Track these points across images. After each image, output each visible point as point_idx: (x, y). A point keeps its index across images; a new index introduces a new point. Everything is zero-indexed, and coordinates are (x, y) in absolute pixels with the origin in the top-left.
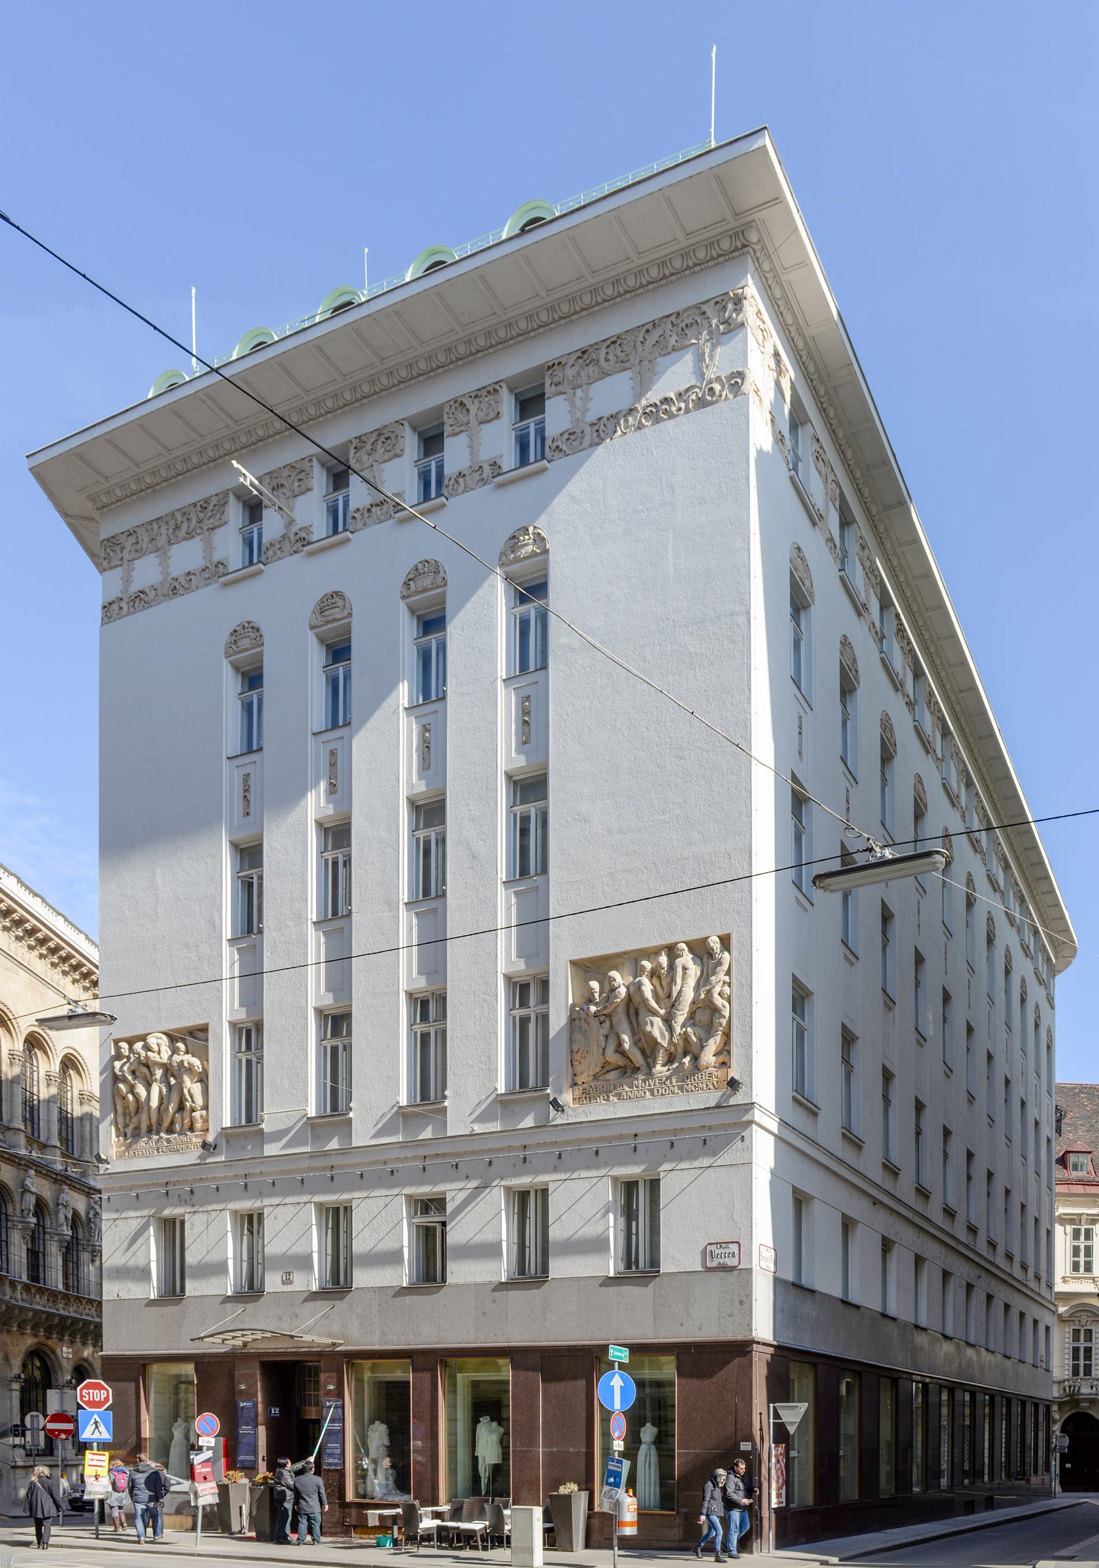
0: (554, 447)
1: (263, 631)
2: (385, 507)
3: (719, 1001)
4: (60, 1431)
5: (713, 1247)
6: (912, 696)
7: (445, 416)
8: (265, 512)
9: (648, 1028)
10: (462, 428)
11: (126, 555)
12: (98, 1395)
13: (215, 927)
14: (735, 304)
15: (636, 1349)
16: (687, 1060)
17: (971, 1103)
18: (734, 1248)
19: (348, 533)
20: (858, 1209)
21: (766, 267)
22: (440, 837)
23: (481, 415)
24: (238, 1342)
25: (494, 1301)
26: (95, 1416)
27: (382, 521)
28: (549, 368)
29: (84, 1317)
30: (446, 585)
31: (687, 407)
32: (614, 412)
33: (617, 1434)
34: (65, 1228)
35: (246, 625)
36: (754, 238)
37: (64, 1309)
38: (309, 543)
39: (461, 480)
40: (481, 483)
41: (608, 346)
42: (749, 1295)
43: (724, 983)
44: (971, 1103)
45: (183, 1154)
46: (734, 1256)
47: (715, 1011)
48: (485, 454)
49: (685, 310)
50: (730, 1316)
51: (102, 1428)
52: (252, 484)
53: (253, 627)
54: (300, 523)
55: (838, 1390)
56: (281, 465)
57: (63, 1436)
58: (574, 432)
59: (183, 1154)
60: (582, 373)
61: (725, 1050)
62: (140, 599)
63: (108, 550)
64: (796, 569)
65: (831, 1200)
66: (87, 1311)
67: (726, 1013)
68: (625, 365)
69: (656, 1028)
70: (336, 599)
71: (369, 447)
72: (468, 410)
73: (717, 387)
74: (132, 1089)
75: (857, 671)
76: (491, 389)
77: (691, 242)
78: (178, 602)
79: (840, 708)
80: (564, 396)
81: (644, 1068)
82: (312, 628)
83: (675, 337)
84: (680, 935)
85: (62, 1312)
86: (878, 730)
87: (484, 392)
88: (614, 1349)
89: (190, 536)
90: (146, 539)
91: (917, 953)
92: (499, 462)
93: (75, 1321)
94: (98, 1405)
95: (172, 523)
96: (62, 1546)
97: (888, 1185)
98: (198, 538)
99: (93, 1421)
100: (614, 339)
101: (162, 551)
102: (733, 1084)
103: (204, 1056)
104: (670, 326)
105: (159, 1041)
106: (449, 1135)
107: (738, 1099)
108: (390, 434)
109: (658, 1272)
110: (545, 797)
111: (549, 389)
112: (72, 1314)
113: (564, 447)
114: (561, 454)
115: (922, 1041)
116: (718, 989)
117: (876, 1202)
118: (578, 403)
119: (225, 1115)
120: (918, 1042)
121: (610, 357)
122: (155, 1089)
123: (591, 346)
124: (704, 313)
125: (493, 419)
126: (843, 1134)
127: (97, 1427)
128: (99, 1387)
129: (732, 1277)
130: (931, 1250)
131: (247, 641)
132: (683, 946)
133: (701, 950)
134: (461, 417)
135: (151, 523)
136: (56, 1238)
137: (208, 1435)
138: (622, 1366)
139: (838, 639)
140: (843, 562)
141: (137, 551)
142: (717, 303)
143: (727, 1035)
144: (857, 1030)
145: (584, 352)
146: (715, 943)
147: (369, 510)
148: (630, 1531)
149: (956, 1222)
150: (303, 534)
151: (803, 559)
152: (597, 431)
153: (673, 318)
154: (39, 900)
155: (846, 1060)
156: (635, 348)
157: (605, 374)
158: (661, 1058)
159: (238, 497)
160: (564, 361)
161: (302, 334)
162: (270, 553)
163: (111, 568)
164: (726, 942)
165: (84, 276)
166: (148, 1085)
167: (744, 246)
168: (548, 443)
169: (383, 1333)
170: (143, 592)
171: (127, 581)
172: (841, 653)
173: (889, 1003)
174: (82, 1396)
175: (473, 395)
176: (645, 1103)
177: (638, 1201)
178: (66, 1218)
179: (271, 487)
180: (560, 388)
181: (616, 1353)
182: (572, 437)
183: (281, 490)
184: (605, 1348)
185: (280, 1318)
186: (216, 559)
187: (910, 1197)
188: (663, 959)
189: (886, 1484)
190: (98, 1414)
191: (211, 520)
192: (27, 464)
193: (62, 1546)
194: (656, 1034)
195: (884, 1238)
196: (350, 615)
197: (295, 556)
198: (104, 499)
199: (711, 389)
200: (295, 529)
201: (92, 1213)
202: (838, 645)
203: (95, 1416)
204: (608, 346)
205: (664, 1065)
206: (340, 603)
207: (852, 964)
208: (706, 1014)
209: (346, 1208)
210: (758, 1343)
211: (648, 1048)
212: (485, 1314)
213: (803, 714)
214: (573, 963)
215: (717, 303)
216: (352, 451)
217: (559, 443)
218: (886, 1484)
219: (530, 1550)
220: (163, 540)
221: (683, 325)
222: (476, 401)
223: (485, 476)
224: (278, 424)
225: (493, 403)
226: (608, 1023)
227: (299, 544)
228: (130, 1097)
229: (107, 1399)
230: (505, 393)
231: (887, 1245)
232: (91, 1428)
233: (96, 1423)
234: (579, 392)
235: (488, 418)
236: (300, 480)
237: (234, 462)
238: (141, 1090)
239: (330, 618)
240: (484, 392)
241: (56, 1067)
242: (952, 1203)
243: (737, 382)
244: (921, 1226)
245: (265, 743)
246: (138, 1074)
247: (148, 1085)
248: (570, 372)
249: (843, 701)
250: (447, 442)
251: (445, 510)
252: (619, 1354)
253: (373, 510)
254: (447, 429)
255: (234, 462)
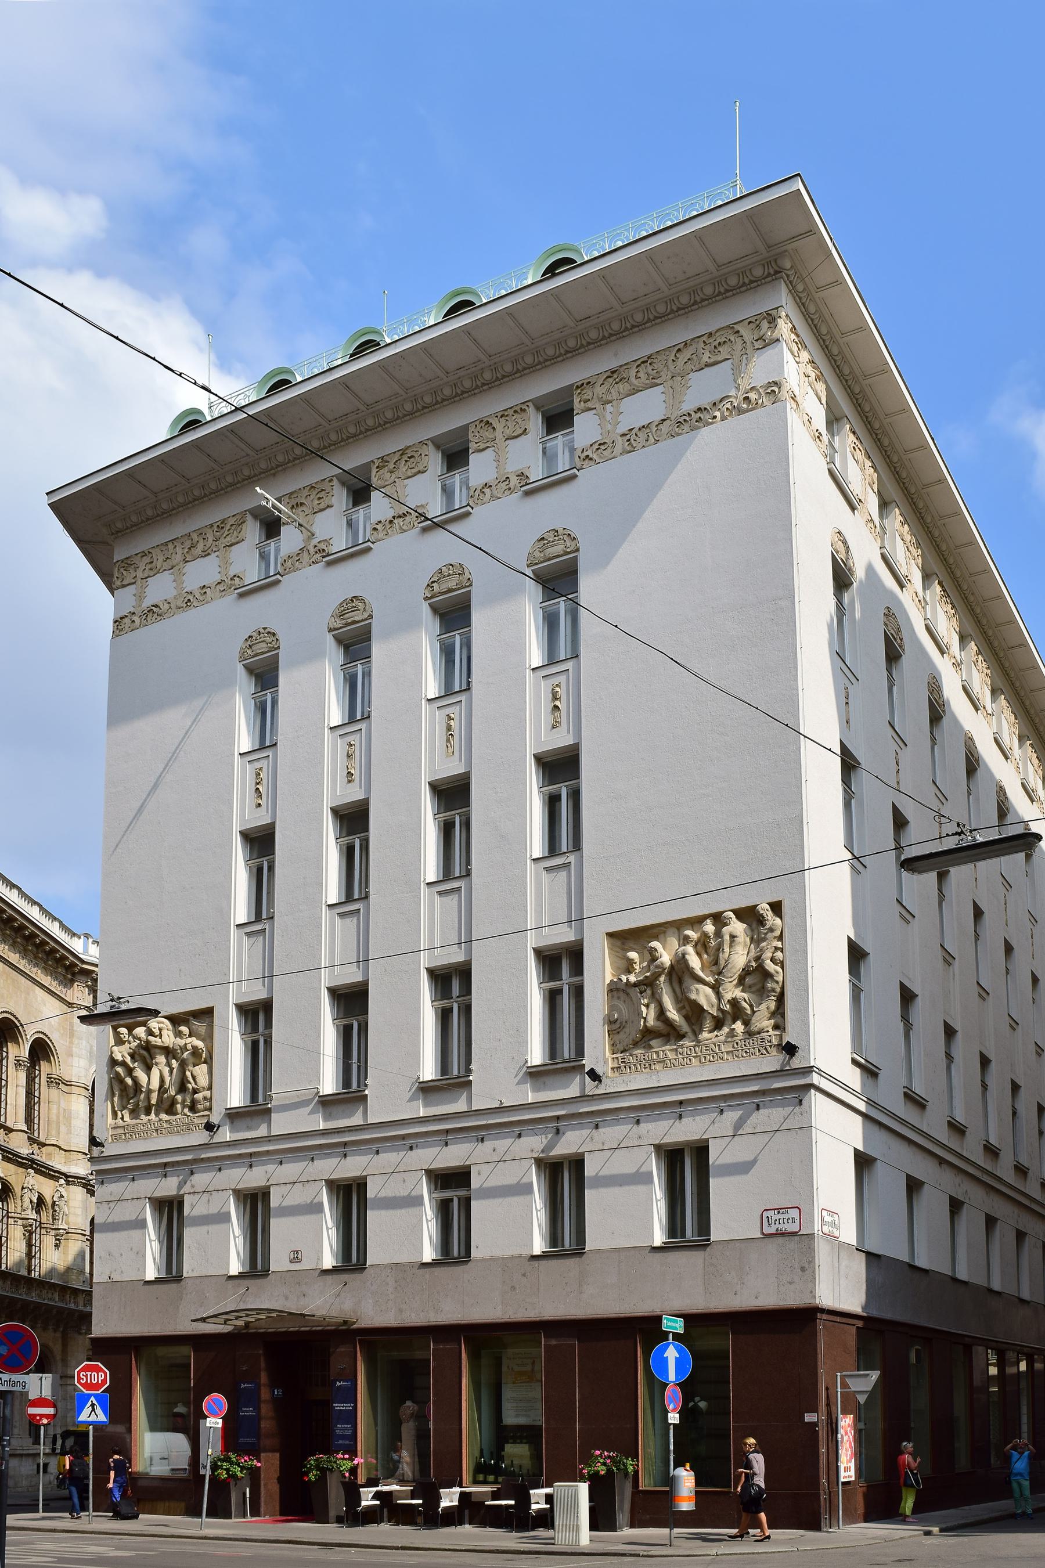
0: (583, 456)
1: (279, 636)
2: (408, 519)
3: (770, 966)
4: (42, 1416)
5: (770, 1214)
6: (958, 658)
7: (471, 435)
8: (283, 529)
9: (693, 996)
10: (488, 445)
11: (140, 574)
12: (96, 1378)
13: (224, 912)
14: (770, 323)
15: (691, 1319)
16: (739, 1027)
17: (1039, 1055)
18: (794, 1213)
19: (369, 543)
20: (923, 1169)
21: (800, 287)
22: (464, 818)
23: (508, 432)
24: (240, 1323)
25: (524, 1275)
26: (93, 1399)
27: (405, 531)
28: (578, 387)
29: (46, 1302)
30: (471, 585)
31: (722, 414)
32: (645, 423)
33: (671, 1407)
34: (29, 1211)
35: (262, 631)
36: (788, 265)
37: (27, 1294)
38: (328, 555)
39: (487, 490)
40: (507, 492)
41: (639, 366)
42: (811, 1262)
43: (776, 949)
44: (1039, 1055)
45: (180, 1135)
46: (793, 1222)
47: (767, 975)
48: (512, 467)
49: (718, 331)
50: (790, 1283)
51: (99, 1410)
52: (273, 506)
53: (269, 633)
54: (320, 535)
55: (908, 1357)
56: (301, 486)
57: (45, 1421)
58: (605, 443)
59: (180, 1135)
60: (612, 391)
61: (779, 1012)
62: (153, 612)
63: (122, 570)
64: (837, 552)
65: (897, 1161)
66: (50, 1296)
67: (779, 978)
68: (658, 381)
69: (703, 995)
70: (356, 603)
71: (391, 466)
72: (494, 428)
73: (753, 396)
74: (130, 1071)
75: (901, 640)
76: (518, 408)
77: (722, 272)
78: (192, 612)
79: (885, 673)
80: (594, 411)
81: (690, 1034)
82: (330, 630)
83: (707, 354)
84: (725, 903)
85: (24, 1297)
86: (926, 693)
87: (511, 412)
88: (667, 1319)
89: (206, 554)
90: (161, 558)
91: (976, 907)
92: (526, 473)
93: (39, 1306)
94: (97, 1386)
95: (188, 544)
96: (54, 1531)
97: (953, 1143)
98: (213, 555)
99: (90, 1403)
100: (645, 359)
101: (177, 568)
102: (790, 1049)
103: (208, 1038)
104: (702, 345)
105: (161, 1025)
106: (473, 1109)
107: (797, 1063)
108: (413, 454)
109: (709, 1240)
110: (577, 776)
111: (577, 405)
112: (34, 1299)
113: (595, 457)
114: (591, 463)
115: (984, 994)
116: (768, 954)
117: (942, 1161)
118: (609, 417)
119: (236, 1096)
120: (980, 995)
121: (641, 374)
122: (155, 1073)
123: (621, 366)
124: (738, 332)
125: (520, 435)
126: (905, 1093)
127: (93, 1410)
128: (98, 1370)
129: (792, 1244)
130: (1001, 1209)
131: (264, 645)
132: (731, 914)
133: (749, 915)
134: (488, 434)
135: (166, 544)
136: (20, 1222)
137: (216, 1416)
138: (677, 1337)
139: (883, 611)
140: (883, 540)
141: (151, 569)
142: (750, 323)
143: (781, 999)
144: (915, 988)
145: (613, 372)
146: (764, 909)
147: (391, 522)
148: (686, 1505)
149: (1029, 1179)
150: (323, 546)
151: (845, 542)
152: (629, 440)
153: (704, 338)
154: (15, 892)
155: (905, 1018)
156: (666, 365)
157: (636, 391)
158: (708, 1024)
159: (255, 517)
160: (593, 381)
161: (327, 374)
162: (289, 564)
163: (124, 586)
164: (776, 908)
165: (62, 305)
166: (148, 1069)
167: (777, 272)
168: (578, 453)
169: (401, 1311)
170: (156, 606)
171: (140, 597)
172: (885, 624)
173: (948, 959)
174: (79, 1378)
175: (499, 415)
176: (691, 1070)
177: (686, 1169)
178: (31, 1202)
179: (290, 505)
180: (589, 405)
181: (669, 1324)
182: (602, 447)
183: (301, 508)
184: (658, 1319)
185: (287, 1298)
186: (231, 574)
187: (978, 1156)
188: (709, 927)
189: (963, 1462)
190: (96, 1396)
191: (228, 539)
192: (45, 501)
193: (54, 1531)
194: (703, 1002)
195: (952, 1198)
196: (371, 617)
197: (313, 566)
198: (119, 525)
199: (746, 399)
200: (315, 542)
201: (57, 1195)
202: (882, 617)
203: (93, 1399)
204: (639, 366)
205: (710, 1032)
206: (361, 606)
207: (908, 922)
208: (756, 977)
209: (359, 1185)
210: (822, 1310)
211: (694, 1013)
212: (513, 1288)
213: (848, 684)
214: (610, 935)
215: (750, 323)
216: (374, 471)
217: (589, 453)
218: (963, 1462)
219: (576, 1529)
220: (179, 557)
221: (716, 343)
222: (503, 420)
223: (512, 485)
224: (298, 451)
225: (520, 421)
226: (649, 992)
227: (318, 556)
228: (129, 1081)
229: (104, 1381)
230: (531, 410)
231: (956, 1206)
232: (87, 1410)
233: (93, 1405)
234: (609, 407)
235: (515, 434)
236: (319, 498)
237: (258, 489)
238: (141, 1075)
239: (349, 621)
240: (511, 412)
241: (25, 1052)
242: (1024, 1161)
243: (773, 391)
244: (991, 1185)
245: (281, 739)
246: (136, 1056)
247: (148, 1069)
248: (599, 390)
249: (889, 670)
250: (472, 458)
251: (471, 517)
252: (674, 1325)
253: (396, 521)
254: (472, 446)
255: (258, 489)
